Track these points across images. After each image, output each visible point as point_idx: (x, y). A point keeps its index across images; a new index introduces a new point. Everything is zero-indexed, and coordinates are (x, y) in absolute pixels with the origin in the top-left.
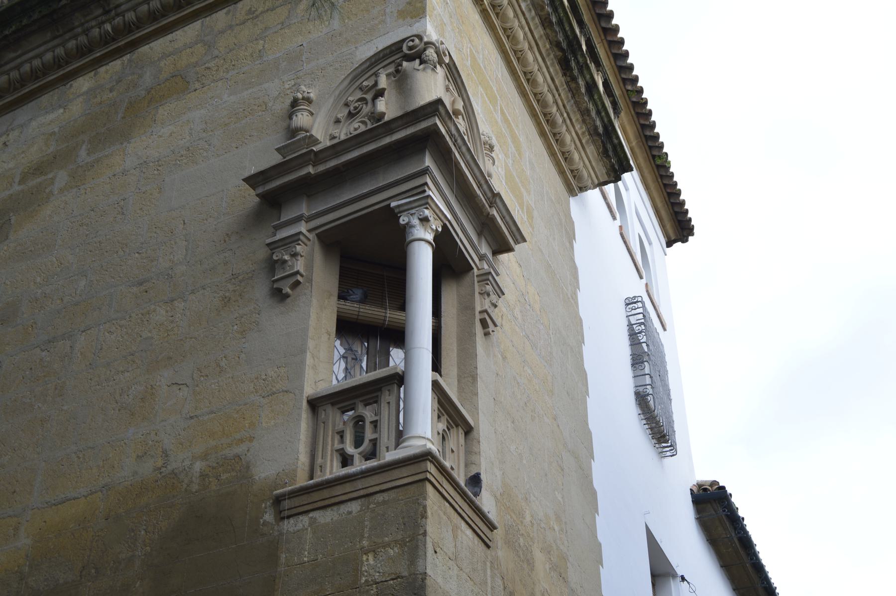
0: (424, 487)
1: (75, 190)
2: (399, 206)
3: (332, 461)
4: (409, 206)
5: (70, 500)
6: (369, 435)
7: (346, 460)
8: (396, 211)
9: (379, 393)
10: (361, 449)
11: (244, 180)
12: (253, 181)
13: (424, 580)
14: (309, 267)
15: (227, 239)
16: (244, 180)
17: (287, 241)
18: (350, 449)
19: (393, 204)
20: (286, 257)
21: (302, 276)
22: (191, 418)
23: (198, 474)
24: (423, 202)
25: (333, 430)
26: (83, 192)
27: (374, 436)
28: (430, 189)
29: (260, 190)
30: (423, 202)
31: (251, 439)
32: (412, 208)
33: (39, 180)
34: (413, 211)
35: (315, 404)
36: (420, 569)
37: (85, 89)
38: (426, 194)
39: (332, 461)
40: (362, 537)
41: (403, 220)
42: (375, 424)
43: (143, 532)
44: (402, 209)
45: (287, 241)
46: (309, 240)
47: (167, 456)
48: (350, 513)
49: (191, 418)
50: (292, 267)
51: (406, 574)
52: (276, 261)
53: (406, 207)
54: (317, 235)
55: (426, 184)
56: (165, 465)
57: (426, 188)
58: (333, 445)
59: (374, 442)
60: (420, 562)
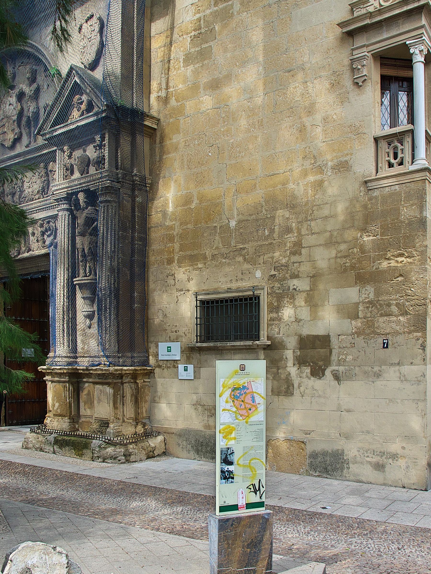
0: (425, 182)
1: (245, 13)
2: (410, 44)
3: (385, 165)
4: (415, 44)
5: (276, 174)
6: (400, 155)
7: (391, 165)
8: (409, 46)
9: (404, 136)
10: (397, 161)
11: (338, 25)
12: (341, 25)
13: (426, 219)
14: (369, 71)
15: (328, 51)
16: (338, 25)
17: (359, 59)
18: (393, 161)
19: (407, 43)
20: (359, 67)
21: (367, 76)
22: (324, 142)
23: (330, 168)
24: (421, 42)
25: (385, 151)
26: (250, 15)
27: (402, 155)
28: (424, 36)
29: (345, 30)
30: (421, 42)
31: (351, 154)
32: (416, 45)
33: (225, 5)
34: (416, 46)
35: (376, 140)
36: (424, 215)
37: (143, 540)
38: (423, 38)
39: (385, 165)
40: (401, 200)
41: (412, 51)
42: (402, 150)
43: (310, 191)
44: (411, 45)
45: (359, 59)
46: (368, 57)
47: (315, 158)
48: (396, 190)
49: (324, 142)
50: (362, 72)
51: (419, 216)
52: (355, 68)
53: (413, 44)
54: (372, 54)
55: (423, 33)
56: (315, 163)
57: (423, 36)
58: (385, 158)
59: (402, 159)
60: (424, 213)
